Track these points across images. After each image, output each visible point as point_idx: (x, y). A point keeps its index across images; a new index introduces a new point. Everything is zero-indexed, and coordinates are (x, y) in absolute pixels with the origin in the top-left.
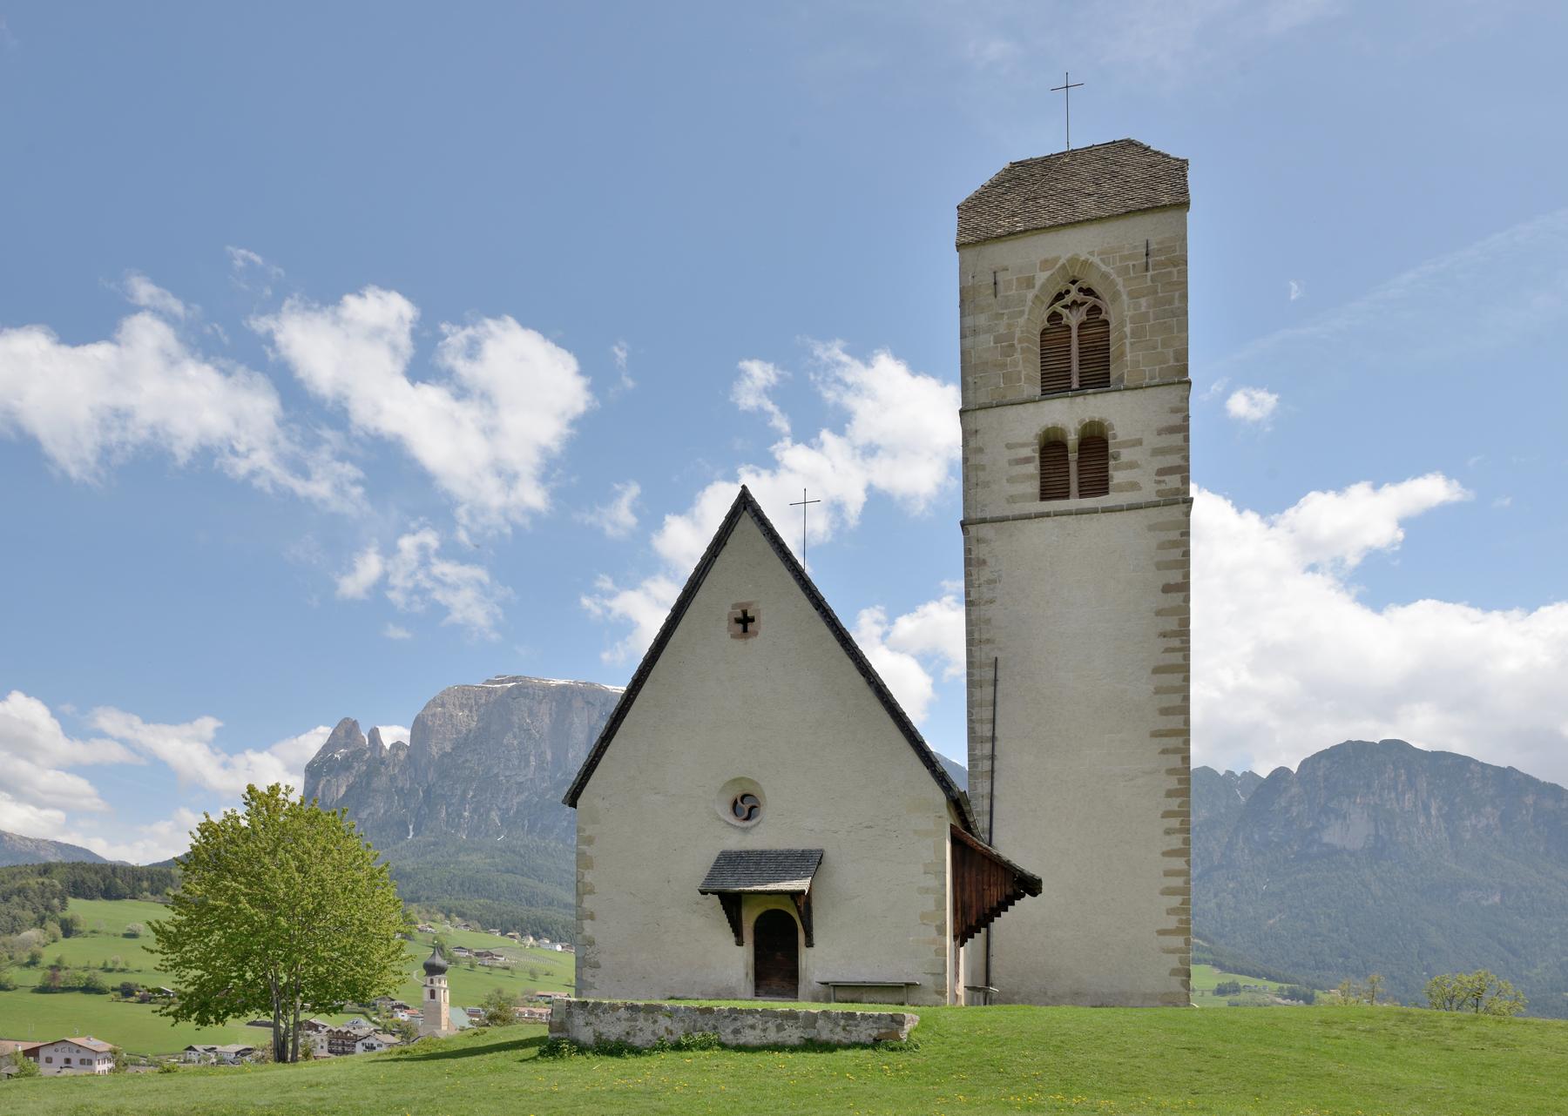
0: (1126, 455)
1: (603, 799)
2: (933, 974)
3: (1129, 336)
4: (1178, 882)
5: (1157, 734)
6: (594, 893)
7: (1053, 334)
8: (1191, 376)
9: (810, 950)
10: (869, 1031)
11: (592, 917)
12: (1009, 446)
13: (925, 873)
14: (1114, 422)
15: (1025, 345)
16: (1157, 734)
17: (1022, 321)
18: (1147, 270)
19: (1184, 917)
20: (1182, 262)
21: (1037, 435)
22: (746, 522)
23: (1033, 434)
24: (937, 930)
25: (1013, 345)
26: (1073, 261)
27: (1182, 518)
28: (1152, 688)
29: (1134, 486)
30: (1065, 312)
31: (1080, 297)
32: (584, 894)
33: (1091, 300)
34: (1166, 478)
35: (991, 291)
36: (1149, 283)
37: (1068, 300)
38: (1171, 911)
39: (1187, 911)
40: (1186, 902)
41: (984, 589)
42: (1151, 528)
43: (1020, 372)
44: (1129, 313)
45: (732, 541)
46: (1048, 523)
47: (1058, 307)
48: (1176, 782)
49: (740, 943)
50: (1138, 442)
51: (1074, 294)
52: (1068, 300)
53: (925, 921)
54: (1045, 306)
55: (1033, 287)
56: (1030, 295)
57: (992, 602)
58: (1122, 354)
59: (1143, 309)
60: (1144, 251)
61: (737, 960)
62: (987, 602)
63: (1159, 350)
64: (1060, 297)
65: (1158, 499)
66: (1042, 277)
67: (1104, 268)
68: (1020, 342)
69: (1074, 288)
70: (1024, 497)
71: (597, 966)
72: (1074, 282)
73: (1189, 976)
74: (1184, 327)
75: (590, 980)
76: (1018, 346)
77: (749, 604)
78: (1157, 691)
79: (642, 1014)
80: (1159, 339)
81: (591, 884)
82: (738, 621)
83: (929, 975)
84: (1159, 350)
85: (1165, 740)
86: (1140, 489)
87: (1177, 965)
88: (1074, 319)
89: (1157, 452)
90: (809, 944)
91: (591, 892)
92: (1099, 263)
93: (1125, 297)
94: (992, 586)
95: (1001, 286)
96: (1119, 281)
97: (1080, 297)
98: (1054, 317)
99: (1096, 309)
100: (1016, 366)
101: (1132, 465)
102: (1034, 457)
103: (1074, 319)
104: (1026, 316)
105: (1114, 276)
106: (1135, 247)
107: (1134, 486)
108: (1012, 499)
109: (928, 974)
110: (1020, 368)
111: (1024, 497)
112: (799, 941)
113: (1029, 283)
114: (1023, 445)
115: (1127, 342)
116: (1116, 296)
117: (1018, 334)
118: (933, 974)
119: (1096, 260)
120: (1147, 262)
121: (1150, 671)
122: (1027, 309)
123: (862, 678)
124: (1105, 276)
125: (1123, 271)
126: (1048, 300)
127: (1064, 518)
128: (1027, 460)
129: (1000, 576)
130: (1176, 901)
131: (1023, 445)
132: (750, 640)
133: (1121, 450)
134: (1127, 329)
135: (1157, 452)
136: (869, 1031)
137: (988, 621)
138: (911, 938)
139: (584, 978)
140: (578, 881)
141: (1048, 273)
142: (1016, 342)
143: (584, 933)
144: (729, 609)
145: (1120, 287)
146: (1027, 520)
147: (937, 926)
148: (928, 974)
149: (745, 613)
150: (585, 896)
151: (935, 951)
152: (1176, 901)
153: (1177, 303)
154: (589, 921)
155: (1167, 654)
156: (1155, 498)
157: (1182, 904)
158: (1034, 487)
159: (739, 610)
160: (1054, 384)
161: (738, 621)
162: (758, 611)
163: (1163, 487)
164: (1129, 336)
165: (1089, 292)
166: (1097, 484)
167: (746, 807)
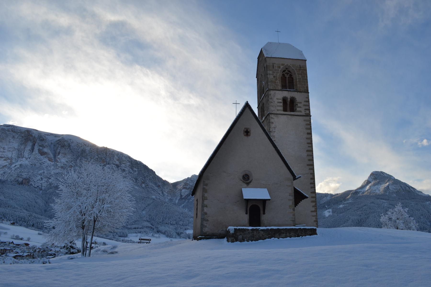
0: (299, 105)
1: (211, 174)
2: (293, 221)
3: (298, 82)
4: (314, 199)
5: (308, 165)
6: (207, 200)
7: (283, 78)
8: (309, 92)
9: (264, 215)
10: (309, 233)
11: (206, 206)
12: (277, 99)
13: (290, 196)
14: (296, 98)
15: (279, 79)
16: (308, 165)
17: (279, 74)
18: (300, 70)
19: (316, 208)
20: (306, 70)
21: (282, 98)
22: (247, 110)
23: (282, 97)
24: (293, 210)
25: (277, 79)
26: (287, 65)
27: (309, 119)
28: (306, 155)
29: (300, 111)
30: (285, 74)
31: (288, 72)
32: (204, 200)
33: (290, 73)
34: (306, 111)
35: (272, 67)
36: (301, 73)
37: (286, 72)
38: (313, 206)
39: (316, 206)
40: (316, 204)
41: (273, 129)
42: (305, 120)
43: (278, 84)
44: (298, 78)
45: (244, 113)
46: (285, 116)
47: (284, 73)
48: (312, 176)
49: (246, 213)
50: (301, 103)
51: (287, 72)
52: (286, 72)
53: (290, 208)
54: (282, 72)
55: (280, 68)
56: (280, 70)
57: (275, 132)
58: (297, 85)
59: (300, 77)
60: (299, 66)
61: (246, 218)
62: (274, 132)
63: (303, 86)
64: (284, 71)
65: (305, 115)
66: (282, 67)
67: (293, 68)
68: (278, 78)
69: (287, 70)
70: (280, 110)
71: (207, 220)
72: (287, 69)
73: (317, 222)
74: (307, 82)
75: (206, 225)
76: (278, 79)
77: (248, 128)
78: (308, 155)
79: (255, 231)
80: (303, 83)
81: (207, 197)
82: (245, 132)
83: (291, 221)
84: (303, 86)
85: (310, 166)
86: (302, 112)
87: (315, 219)
88: (287, 76)
89: (304, 105)
90: (264, 213)
91: (207, 199)
92: (292, 67)
93: (297, 74)
94: (275, 128)
95: (274, 67)
96: (296, 71)
97: (288, 72)
98: (283, 75)
99: (291, 75)
100: (278, 83)
101: (300, 107)
102: (282, 102)
103: (287, 76)
104: (279, 74)
105: (295, 70)
106: (298, 66)
107: (300, 111)
108: (278, 110)
109: (291, 221)
110: (279, 83)
111: (280, 110)
112: (261, 213)
113: (279, 67)
114: (280, 99)
115: (298, 83)
116: (295, 74)
117: (278, 77)
118: (293, 221)
119: (291, 66)
120: (300, 69)
121: (306, 151)
122: (279, 72)
123: (274, 148)
124: (293, 69)
125: (296, 69)
126: (282, 71)
127: (288, 116)
128: (281, 102)
129: (276, 126)
130: (314, 204)
131: (280, 99)
132: (249, 137)
133: (298, 104)
134: (298, 80)
135: (304, 105)
136: (309, 233)
137: (274, 136)
138: (287, 212)
139: (204, 224)
140: (203, 196)
141: (283, 66)
142: (277, 78)
143: (204, 211)
144: (244, 129)
145: (296, 72)
146: (281, 115)
147: (293, 209)
148: (291, 221)
149: (247, 130)
150: (205, 200)
151: (293, 215)
152: (314, 204)
153: (306, 78)
154: (206, 207)
155: (309, 148)
156: (304, 114)
157: (315, 205)
158: (282, 108)
159: (246, 129)
160: (284, 87)
161: (245, 132)
162: (250, 130)
163: (306, 112)
164: (298, 82)
165: (289, 71)
166: (293, 109)
167: (246, 178)
